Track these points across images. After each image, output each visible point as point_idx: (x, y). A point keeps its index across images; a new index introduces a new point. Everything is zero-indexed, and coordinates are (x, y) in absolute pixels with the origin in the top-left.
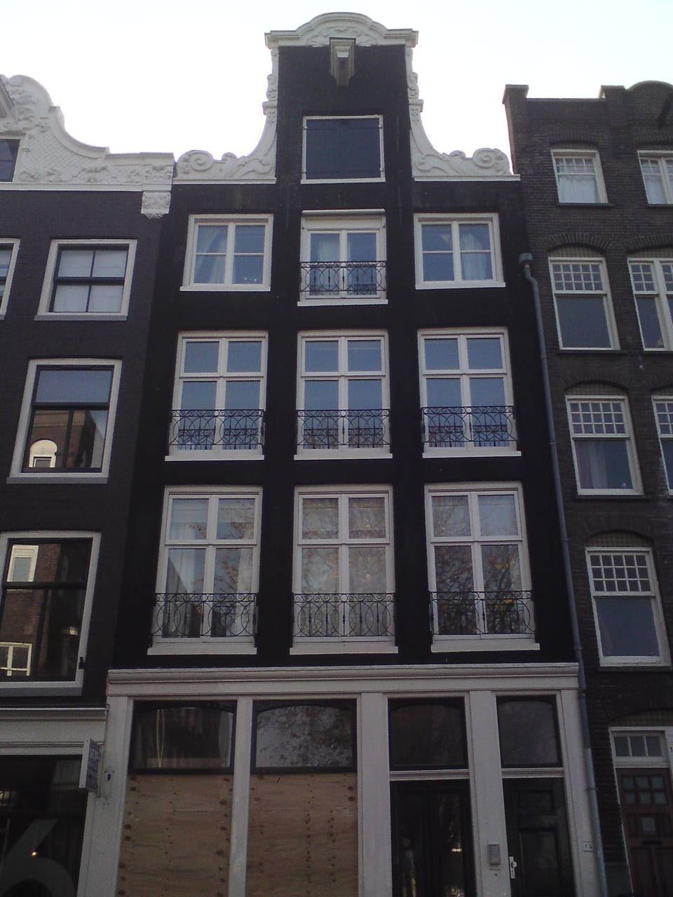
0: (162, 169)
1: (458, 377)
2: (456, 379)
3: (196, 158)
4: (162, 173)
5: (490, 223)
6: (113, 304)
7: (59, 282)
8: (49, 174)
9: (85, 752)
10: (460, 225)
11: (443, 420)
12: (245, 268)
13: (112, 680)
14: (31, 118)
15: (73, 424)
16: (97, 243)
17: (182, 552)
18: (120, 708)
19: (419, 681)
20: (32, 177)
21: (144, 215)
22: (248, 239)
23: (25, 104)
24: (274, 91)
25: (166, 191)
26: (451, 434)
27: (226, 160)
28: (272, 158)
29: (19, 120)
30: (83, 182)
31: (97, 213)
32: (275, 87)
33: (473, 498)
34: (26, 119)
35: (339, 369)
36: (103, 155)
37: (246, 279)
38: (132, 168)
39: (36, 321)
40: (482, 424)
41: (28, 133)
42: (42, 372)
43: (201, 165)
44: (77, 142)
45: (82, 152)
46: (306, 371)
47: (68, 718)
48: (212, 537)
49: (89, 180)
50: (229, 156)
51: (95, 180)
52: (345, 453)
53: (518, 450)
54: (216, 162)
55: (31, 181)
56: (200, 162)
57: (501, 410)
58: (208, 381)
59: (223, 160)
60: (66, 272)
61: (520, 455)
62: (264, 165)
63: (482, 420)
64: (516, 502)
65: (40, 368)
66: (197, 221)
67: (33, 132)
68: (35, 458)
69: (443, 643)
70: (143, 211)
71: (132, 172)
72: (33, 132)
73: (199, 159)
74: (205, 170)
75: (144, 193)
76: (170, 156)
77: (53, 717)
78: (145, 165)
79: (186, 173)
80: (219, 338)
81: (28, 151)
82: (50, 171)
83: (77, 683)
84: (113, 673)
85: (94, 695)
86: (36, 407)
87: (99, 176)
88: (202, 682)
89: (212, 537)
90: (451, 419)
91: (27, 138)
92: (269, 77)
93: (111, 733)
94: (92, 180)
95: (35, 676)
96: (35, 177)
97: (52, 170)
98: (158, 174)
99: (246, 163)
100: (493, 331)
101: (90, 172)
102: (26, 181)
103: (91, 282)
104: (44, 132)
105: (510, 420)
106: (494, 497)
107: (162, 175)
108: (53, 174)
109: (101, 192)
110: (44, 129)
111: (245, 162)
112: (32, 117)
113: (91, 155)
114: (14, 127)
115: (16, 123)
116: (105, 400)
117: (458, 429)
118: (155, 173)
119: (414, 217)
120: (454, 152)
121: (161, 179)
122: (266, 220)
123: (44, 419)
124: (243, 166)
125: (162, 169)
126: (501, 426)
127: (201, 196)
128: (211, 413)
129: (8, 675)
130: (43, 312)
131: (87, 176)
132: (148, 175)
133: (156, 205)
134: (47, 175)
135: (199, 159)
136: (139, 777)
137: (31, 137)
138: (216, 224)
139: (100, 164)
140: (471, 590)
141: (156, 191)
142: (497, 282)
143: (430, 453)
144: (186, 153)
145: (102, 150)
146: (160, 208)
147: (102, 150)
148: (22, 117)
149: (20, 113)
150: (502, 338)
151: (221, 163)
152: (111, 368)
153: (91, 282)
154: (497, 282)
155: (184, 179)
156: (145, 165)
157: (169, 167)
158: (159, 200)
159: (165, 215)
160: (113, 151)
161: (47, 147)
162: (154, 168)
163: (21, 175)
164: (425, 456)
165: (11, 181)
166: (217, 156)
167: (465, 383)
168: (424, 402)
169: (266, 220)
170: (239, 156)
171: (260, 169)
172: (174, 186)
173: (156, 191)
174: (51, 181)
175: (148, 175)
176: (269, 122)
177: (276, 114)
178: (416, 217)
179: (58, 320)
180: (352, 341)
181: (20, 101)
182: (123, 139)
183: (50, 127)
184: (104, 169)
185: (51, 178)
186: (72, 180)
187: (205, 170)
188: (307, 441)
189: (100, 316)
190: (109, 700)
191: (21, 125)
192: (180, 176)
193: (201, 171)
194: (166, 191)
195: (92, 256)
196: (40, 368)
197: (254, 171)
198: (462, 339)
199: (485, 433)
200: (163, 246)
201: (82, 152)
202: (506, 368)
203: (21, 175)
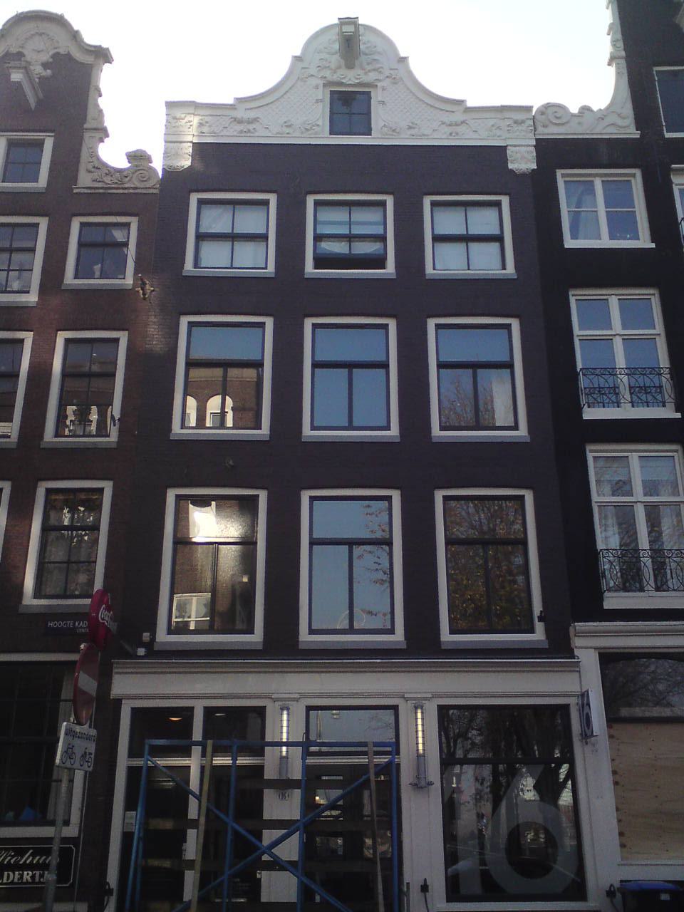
0: (523, 122)
1: (611, 338)
2: (609, 340)
3: (553, 111)
4: (523, 127)
5: (633, 181)
6: (489, 262)
7: (200, 237)
8: (410, 128)
9: (573, 702)
10: (602, 181)
11: (601, 380)
12: (621, 224)
13: (579, 633)
14: (381, 70)
15: (228, 379)
16: (478, 199)
17: (501, 507)
18: (588, 660)
19: (619, 637)
20: (394, 131)
21: (512, 171)
22: (617, 195)
23: (370, 54)
24: (618, 40)
25: (530, 146)
26: (610, 395)
27: (584, 113)
28: (628, 110)
29: (369, 71)
30: (235, 134)
31: (464, 169)
32: (619, 36)
33: (634, 459)
34: (374, 70)
35: (613, 327)
36: (461, 108)
37: (618, 235)
38: (492, 122)
39: (428, 280)
40: (595, 386)
41: (379, 84)
42: (194, 329)
43: (557, 118)
44: (433, 93)
45: (437, 104)
46: (580, 330)
47: (534, 668)
48: (639, 493)
49: (451, 134)
50: (585, 110)
51: (457, 134)
52: (627, 412)
53: (676, 412)
54: (573, 115)
55: (393, 135)
56: (558, 115)
57: (657, 371)
58: (638, 339)
59: (579, 112)
60: (442, 230)
61: (680, 417)
62: (624, 118)
63: (642, 381)
64: (676, 460)
65: (191, 324)
66: (563, 175)
67: (385, 83)
68: (211, 413)
69: (613, 601)
70: (510, 166)
71: (493, 126)
72: (385, 83)
73: (556, 112)
74: (563, 124)
75: (509, 147)
76: (529, 109)
77: (328, 669)
78: (504, 119)
79: (545, 126)
80: (609, 295)
81: (383, 103)
82: (411, 125)
83: (256, 638)
84: (580, 626)
85: (559, 647)
86: (190, 364)
87: (460, 129)
88: (597, 636)
89: (639, 493)
90: (611, 380)
91: (379, 90)
92: (611, 27)
93: (580, 682)
94: (453, 134)
95: (211, 630)
96: (397, 131)
97: (412, 123)
98: (520, 128)
99: (605, 116)
100: (594, 293)
101: (450, 125)
102: (387, 135)
103: (233, 237)
104: (396, 83)
105: (665, 380)
106: (664, 458)
107: (524, 128)
108: (414, 128)
109: (320, 145)
110: (395, 81)
111: (602, 115)
112: (382, 68)
113: (448, 107)
114: (365, 79)
115: (366, 73)
116: (258, 357)
117: (615, 390)
118: (516, 127)
119: (557, 174)
120: (585, 106)
121: (523, 133)
122: (634, 175)
123: (196, 373)
124: (603, 119)
125: (523, 122)
126: (615, 387)
127: (566, 151)
128: (612, 371)
129: (191, 628)
130: (189, 266)
131: (448, 130)
132: (510, 128)
133: (523, 160)
134: (408, 129)
135: (556, 112)
136: (616, 726)
137: (384, 89)
138: (575, 179)
139: (458, 117)
140: (637, 550)
141: (522, 146)
142: (644, 242)
143: (589, 414)
144: (543, 106)
145: (461, 102)
146: (526, 163)
147: (460, 102)
148: (369, 67)
149: (368, 64)
150: (653, 298)
151: (579, 116)
152: (262, 325)
153: (233, 237)
154: (644, 242)
155: (553, 132)
156: (504, 119)
157: (528, 121)
158: (526, 155)
159: (533, 170)
160: (471, 103)
161: (399, 97)
162: (516, 122)
163: (382, 129)
164: (585, 417)
165: (371, 135)
166: (574, 110)
167: (618, 344)
168: (579, 365)
169: (634, 175)
170: (595, 108)
171: (620, 122)
172: (537, 140)
173: (522, 146)
174: (203, 133)
175: (510, 128)
176: (618, 74)
177: (625, 65)
178: (559, 172)
179: (445, 278)
180: (579, 300)
181: (367, 51)
182: (481, 90)
183: (401, 79)
184: (463, 122)
185: (413, 132)
186: (433, 133)
187: (563, 124)
188: (610, 399)
189: (486, 274)
190: (577, 652)
191: (372, 77)
192: (540, 129)
193: (556, 124)
194: (530, 146)
195: (464, 214)
196: (191, 324)
197: (612, 124)
198: (614, 300)
199: (641, 394)
200: (536, 202)
201: (437, 104)
202: (659, 328)
203: (382, 129)
